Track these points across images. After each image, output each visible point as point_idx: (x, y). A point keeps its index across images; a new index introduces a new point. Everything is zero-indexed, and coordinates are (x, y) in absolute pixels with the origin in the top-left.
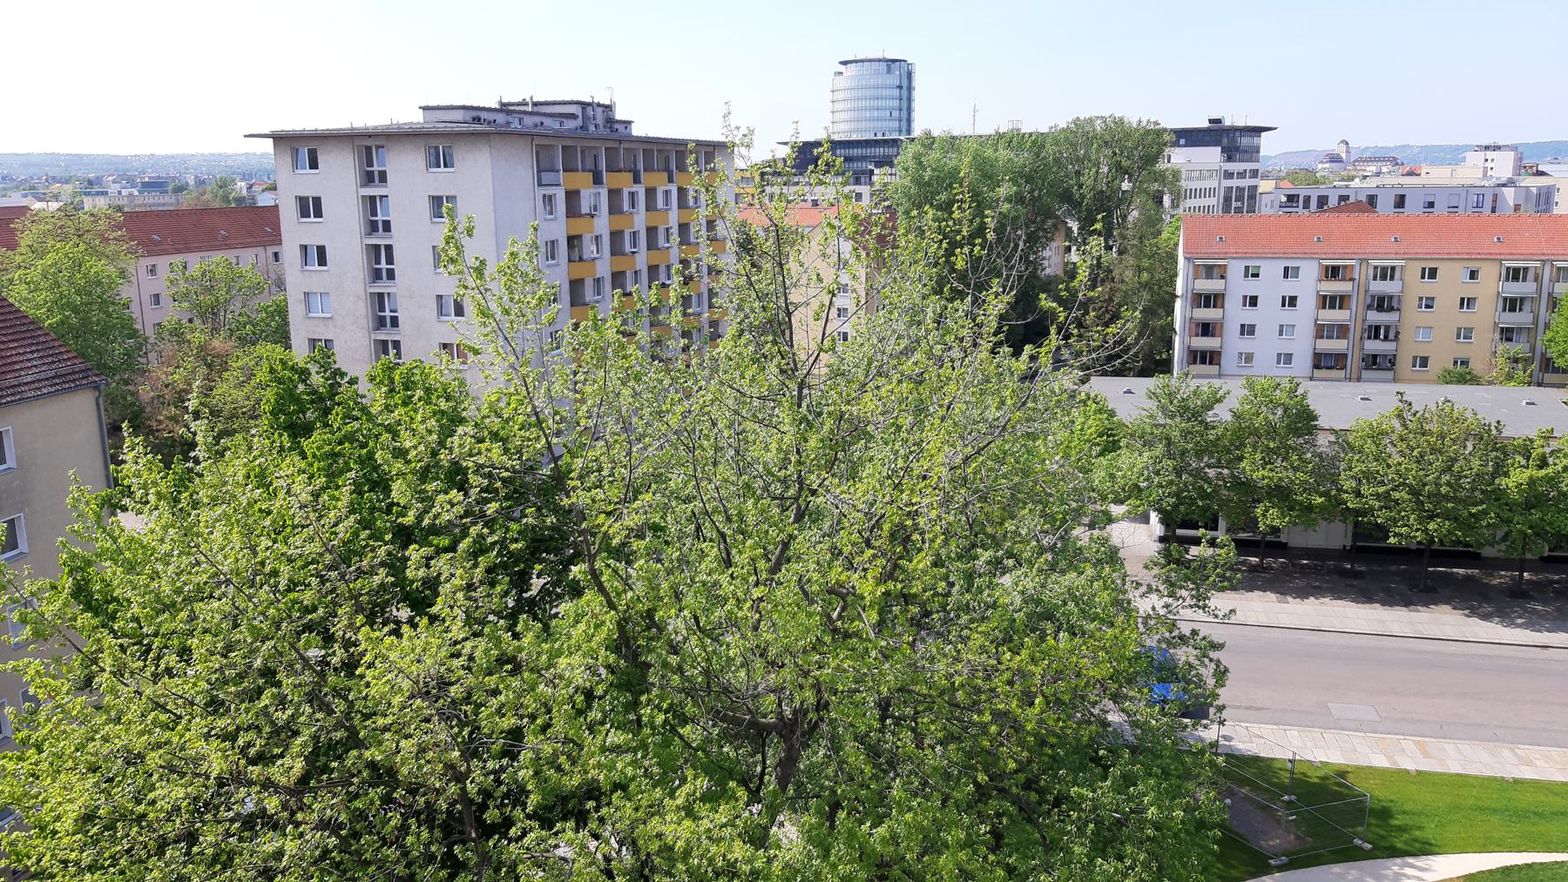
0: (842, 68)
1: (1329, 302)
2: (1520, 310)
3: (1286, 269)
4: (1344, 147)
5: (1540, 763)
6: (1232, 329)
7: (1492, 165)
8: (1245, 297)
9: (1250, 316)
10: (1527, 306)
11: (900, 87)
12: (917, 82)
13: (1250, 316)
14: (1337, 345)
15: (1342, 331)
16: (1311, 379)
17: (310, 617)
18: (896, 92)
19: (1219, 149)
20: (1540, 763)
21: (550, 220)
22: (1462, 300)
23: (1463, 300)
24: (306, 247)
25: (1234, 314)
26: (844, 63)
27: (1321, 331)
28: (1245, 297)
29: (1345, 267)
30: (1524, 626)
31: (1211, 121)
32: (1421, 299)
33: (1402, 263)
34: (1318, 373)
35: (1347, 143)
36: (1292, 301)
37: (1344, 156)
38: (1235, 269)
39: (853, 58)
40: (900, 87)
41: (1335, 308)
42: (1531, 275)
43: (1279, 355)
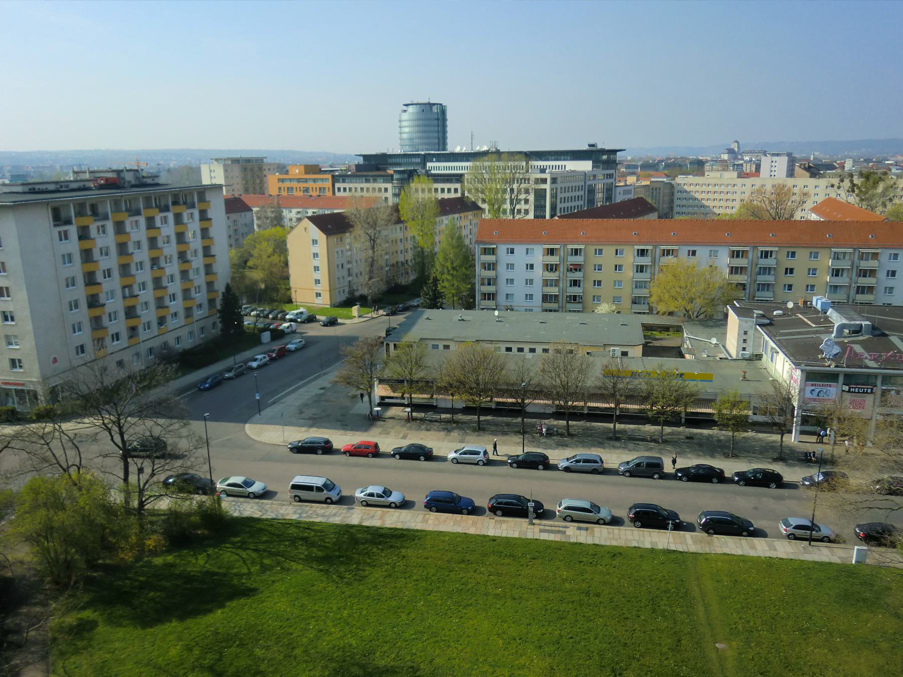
0: (405, 108)
1: (550, 268)
2: (842, 275)
3: (527, 249)
4: (736, 144)
6: (502, 282)
7: (776, 164)
8: (527, 265)
9: (530, 275)
10: (845, 275)
11: (438, 119)
12: (449, 116)
13: (510, 275)
14: (554, 291)
15: (556, 283)
17: (95, 574)
18: (436, 122)
19: (591, 162)
21: (71, 266)
22: (616, 266)
23: (616, 266)
24: (7, 336)
25: (503, 273)
26: (407, 105)
27: (546, 283)
28: (888, 271)
29: (556, 249)
30: (581, 449)
31: (590, 146)
32: (595, 265)
33: (777, 249)
35: (738, 143)
36: (532, 266)
37: (736, 149)
38: (502, 249)
39: (410, 103)
40: (438, 119)
41: (866, 277)
42: (649, 252)
43: (526, 295)
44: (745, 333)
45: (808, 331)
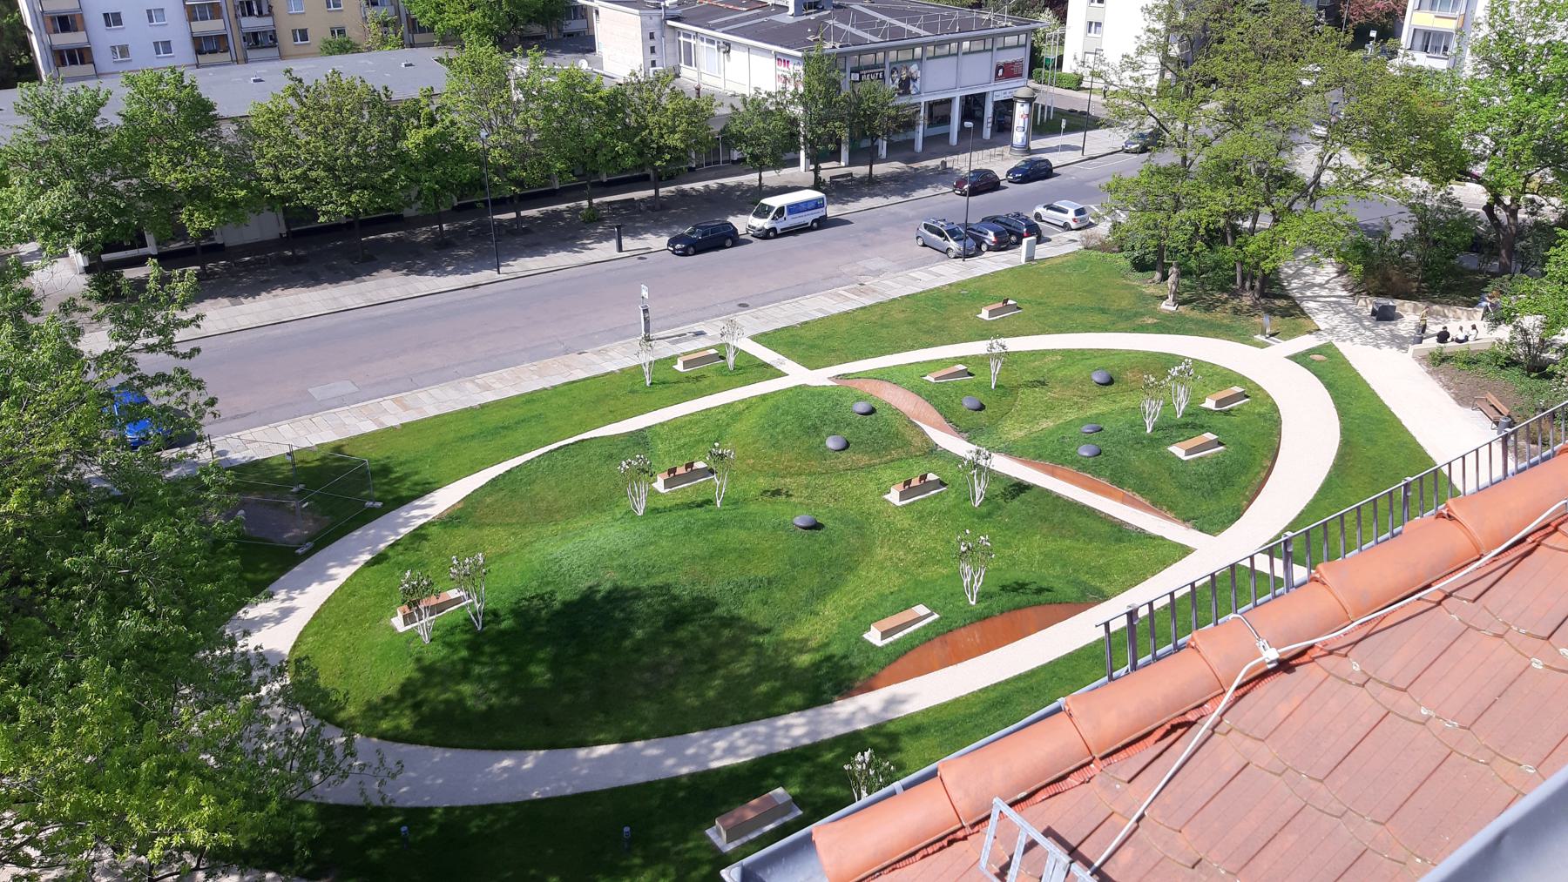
5: (498, 385)
16: (198, 66)
20: (498, 385)
34: (202, 59)
43: (156, 44)
44: (652, 36)
45: (726, 22)
